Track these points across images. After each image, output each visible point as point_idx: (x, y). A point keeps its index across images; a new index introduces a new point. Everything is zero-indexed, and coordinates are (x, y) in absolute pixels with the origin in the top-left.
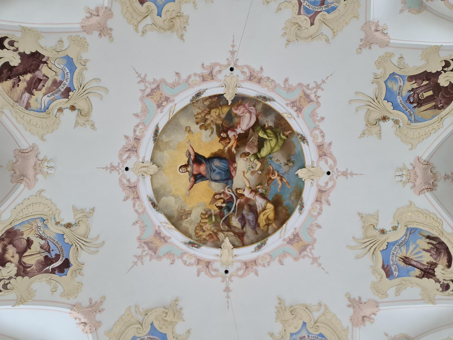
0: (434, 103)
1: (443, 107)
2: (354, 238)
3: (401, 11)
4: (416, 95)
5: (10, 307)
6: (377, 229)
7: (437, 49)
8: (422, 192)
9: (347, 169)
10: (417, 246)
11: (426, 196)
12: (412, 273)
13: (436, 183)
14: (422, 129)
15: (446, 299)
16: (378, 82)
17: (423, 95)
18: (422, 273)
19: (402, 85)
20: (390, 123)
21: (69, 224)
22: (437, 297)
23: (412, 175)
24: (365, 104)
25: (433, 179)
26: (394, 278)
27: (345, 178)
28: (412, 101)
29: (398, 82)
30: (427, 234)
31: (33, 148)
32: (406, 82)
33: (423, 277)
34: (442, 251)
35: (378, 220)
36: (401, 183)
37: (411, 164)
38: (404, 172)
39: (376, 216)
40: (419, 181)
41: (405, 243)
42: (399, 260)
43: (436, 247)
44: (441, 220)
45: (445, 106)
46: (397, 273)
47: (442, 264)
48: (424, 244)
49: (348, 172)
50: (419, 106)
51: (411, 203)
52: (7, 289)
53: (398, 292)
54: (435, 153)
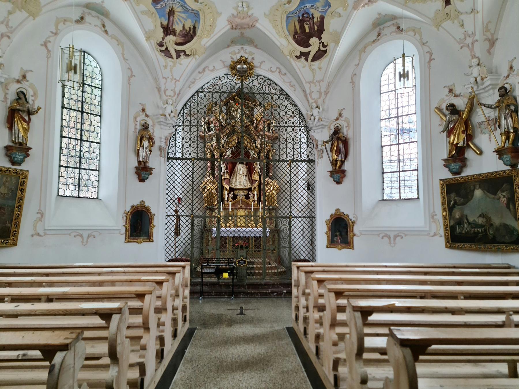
0: (299, 32)
1: (294, 38)
4: (309, 19)
5: (338, 48)
7: (337, 42)
10: (186, 20)
11: (226, 26)
12: (163, 19)
26: (154, 7)
28: (305, 15)
30: (196, 26)
31: (230, 22)
34: (187, 38)
37: (252, 14)
40: (238, 21)
41: (185, 9)
43: (188, 34)
46: (159, 8)
48: (189, 24)
51: (221, 14)
52: (327, 46)
53: (143, 12)
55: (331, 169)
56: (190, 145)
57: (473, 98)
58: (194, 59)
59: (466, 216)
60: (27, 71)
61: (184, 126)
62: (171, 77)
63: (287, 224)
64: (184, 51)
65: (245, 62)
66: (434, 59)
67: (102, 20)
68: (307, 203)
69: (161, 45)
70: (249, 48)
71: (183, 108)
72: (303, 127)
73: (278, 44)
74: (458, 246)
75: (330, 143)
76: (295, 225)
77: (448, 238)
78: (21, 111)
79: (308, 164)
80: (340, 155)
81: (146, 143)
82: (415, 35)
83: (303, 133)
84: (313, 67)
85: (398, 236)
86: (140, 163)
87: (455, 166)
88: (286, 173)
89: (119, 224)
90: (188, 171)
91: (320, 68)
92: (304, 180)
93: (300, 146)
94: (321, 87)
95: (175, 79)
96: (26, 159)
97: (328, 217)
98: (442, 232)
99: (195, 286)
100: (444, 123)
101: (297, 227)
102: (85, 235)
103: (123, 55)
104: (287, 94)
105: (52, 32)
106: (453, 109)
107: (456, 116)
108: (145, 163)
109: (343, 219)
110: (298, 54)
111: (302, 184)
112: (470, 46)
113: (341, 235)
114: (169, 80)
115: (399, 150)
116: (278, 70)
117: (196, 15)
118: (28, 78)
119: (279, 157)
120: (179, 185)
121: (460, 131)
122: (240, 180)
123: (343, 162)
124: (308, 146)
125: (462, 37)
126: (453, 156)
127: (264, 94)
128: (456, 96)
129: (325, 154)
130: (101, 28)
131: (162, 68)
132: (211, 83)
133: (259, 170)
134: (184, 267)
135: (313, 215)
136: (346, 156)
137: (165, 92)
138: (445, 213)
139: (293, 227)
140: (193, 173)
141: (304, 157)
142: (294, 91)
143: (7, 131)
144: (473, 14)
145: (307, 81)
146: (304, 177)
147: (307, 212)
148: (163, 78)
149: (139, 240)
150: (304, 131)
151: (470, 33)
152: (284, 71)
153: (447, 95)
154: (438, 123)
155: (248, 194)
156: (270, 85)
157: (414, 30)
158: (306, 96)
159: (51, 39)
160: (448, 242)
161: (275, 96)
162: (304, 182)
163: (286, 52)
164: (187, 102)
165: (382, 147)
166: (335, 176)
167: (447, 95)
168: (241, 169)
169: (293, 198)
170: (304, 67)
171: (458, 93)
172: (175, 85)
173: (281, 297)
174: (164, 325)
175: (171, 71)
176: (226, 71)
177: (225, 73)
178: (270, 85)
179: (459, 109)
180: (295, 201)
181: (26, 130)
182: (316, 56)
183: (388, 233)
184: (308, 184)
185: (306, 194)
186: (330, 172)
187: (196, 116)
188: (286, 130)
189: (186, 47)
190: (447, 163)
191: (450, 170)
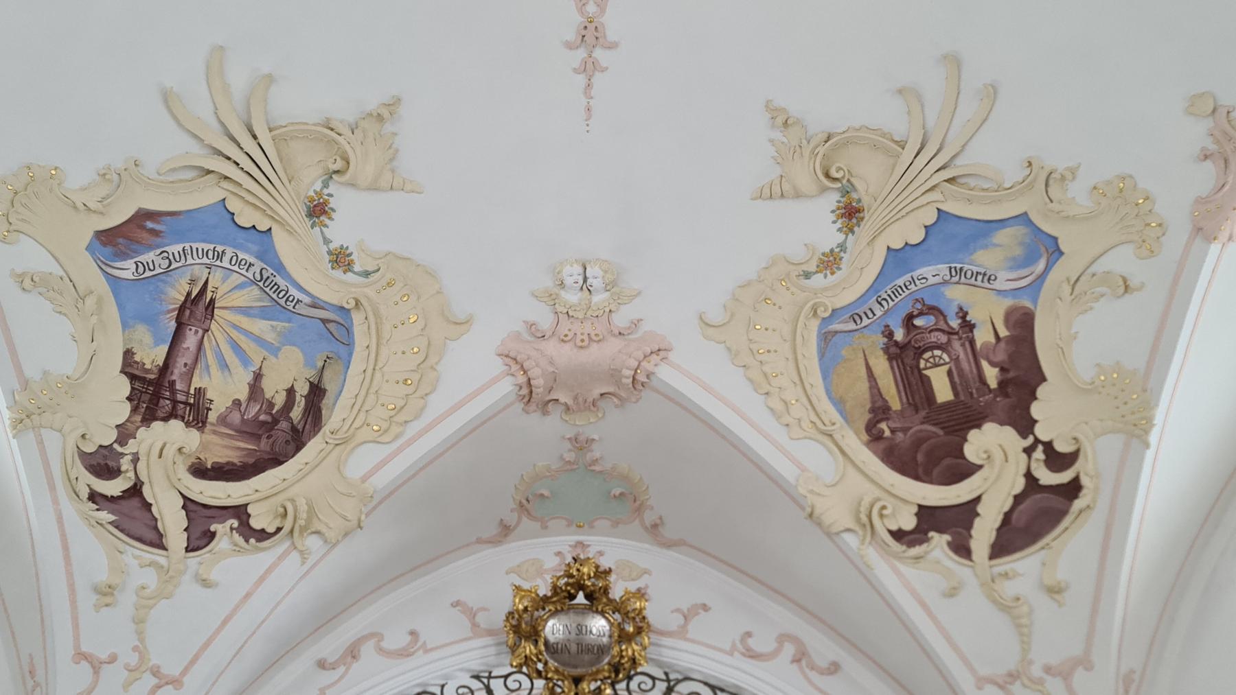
0: (896, 405)
1: (874, 437)
2: (270, 79)
4: (944, 339)
5: (1149, 454)
6: (326, 185)
7: (1136, 428)
8: (515, 367)
9: (613, 46)
10: (275, 351)
11: (495, 380)
13: (556, 412)
14: (791, 364)
15: (64, 449)
16: (1031, 186)
17: (936, 365)
18: (148, 371)
19: (997, 285)
20: (828, 234)
21: (952, 596)
22: (52, 441)
23: (588, 328)
24: (930, 123)
25: (570, 402)
26: (102, 266)
27: (571, 36)
28: (918, 322)
29: (1011, 269)
30: (329, 384)
31: (512, 360)
32: (1008, 302)
33: (133, 378)
34: (264, 444)
35: (374, 188)
36: (548, 283)
37: (636, 324)
38: (598, 298)
39: (388, 181)
40: (563, 355)
41: (276, 295)
42: (193, 282)
43: (276, 421)
44: (397, 437)
45: (882, 445)
46: (128, 275)
47: (204, 446)
48: (286, 373)
49: (598, 53)
50: (893, 350)
51: (464, 324)
53: (27, 281)
54: (686, 409)
58: (295, 555)
62: (133, 659)
64: (240, 512)
84: (1009, 589)
91: (1054, 591)
95: (156, 672)
110: (908, 522)
114: (113, 676)
116: (789, 650)
117: (335, 327)
131: (87, 600)
145: (984, 671)
148: (81, 656)
152: (823, 648)
163: (837, 513)
170: (952, 593)
175: (139, 621)
176: (482, 653)
177: (476, 666)
182: (1019, 519)
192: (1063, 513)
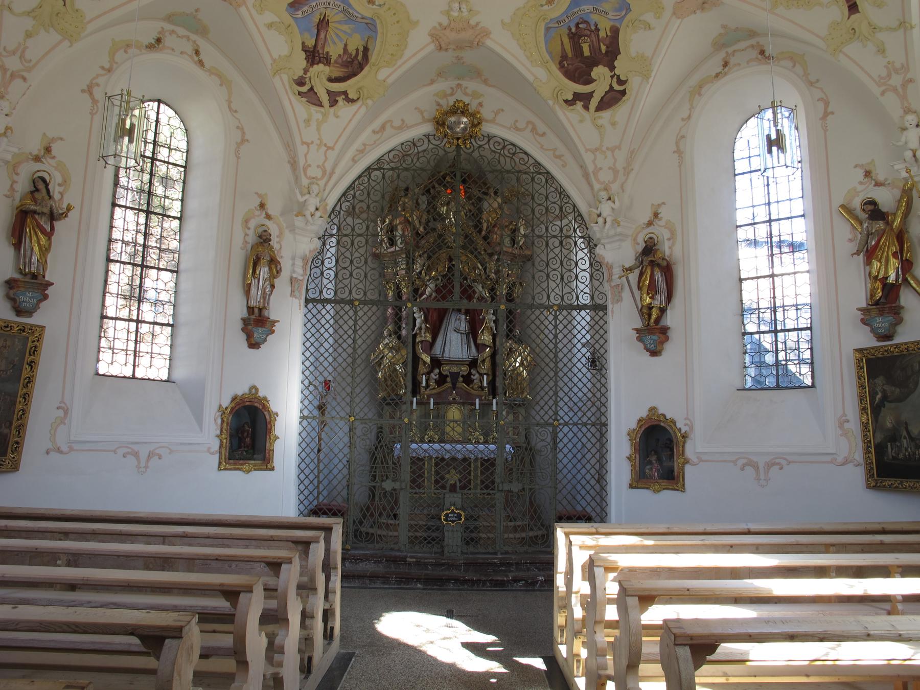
0: (570, 55)
1: (561, 66)
3: (724, 27)
4: (589, 33)
7: (646, 76)
26: (291, 15)
28: (580, 26)
30: (370, 47)
31: (434, 36)
32: (612, 23)
34: (350, 69)
37: (477, 24)
41: (349, 16)
43: (353, 61)
46: (300, 16)
47: (331, 72)
48: (355, 43)
53: (270, 26)
55: (639, 324)
56: (351, 275)
57: (911, 189)
59: (906, 424)
60: (53, 140)
61: (340, 236)
63: (549, 439)
64: (345, 93)
65: (464, 110)
66: (832, 113)
67: (195, 42)
68: (590, 395)
69: (300, 82)
70: (472, 85)
71: (339, 200)
72: (581, 237)
73: (531, 78)
74: (890, 486)
75: (637, 272)
76: (565, 440)
77: (872, 468)
78: (39, 214)
79: (592, 313)
80: (657, 297)
81: (264, 271)
82: (794, 66)
83: (581, 250)
85: (774, 464)
86: (250, 310)
87: (882, 323)
88: (546, 332)
89: (209, 435)
90: (346, 327)
91: (613, 124)
92: (583, 346)
93: (577, 277)
94: (615, 160)
95: (325, 145)
96: (42, 305)
97: (634, 425)
98: (859, 456)
99: (356, 563)
100: (859, 236)
101: (570, 446)
102: (144, 455)
103: (229, 102)
104: (548, 173)
105: (103, 68)
106: (874, 211)
107: (881, 222)
108: (260, 310)
109: (664, 428)
110: (570, 97)
111: (579, 355)
112: (900, 90)
113: (659, 460)
114: (313, 148)
115: (774, 288)
116: (530, 127)
117: (370, 26)
118: (54, 152)
119: (533, 298)
120: (326, 355)
121: (890, 254)
122: (454, 345)
123: (663, 311)
124: (591, 276)
125: (884, 73)
126: (877, 303)
127: (501, 172)
128: (878, 184)
129: (626, 294)
130: (191, 56)
131: (302, 125)
132: (397, 152)
133: (493, 325)
134: (328, 530)
135: (603, 419)
136: (669, 298)
137: (305, 169)
138: (864, 418)
139: (561, 445)
140: (355, 331)
141: (585, 300)
142: (563, 166)
143: (10, 252)
144: (902, 30)
146: (584, 341)
147: (589, 414)
148: (303, 143)
149: (246, 467)
150: (583, 246)
151: (898, 65)
152: (541, 127)
153: (861, 183)
154: (846, 236)
155: (470, 374)
156: (514, 154)
157: (791, 59)
158: (586, 176)
159: (101, 80)
160: (872, 476)
161: (524, 176)
162: (584, 350)
164: (348, 188)
165: (741, 280)
166: (649, 339)
167: (861, 183)
168: (457, 324)
169: (561, 384)
170: (581, 121)
171: (881, 178)
172: (326, 158)
173: (534, 590)
174: (282, 666)
175: (318, 129)
178: (514, 154)
179: (884, 210)
180: (566, 389)
181: (44, 251)
183: (755, 458)
184: (593, 354)
185: (589, 375)
186: (638, 330)
187: (364, 216)
188: (547, 245)
189: (349, 86)
190: (867, 315)
191: (873, 331)
192: (620, 99)
